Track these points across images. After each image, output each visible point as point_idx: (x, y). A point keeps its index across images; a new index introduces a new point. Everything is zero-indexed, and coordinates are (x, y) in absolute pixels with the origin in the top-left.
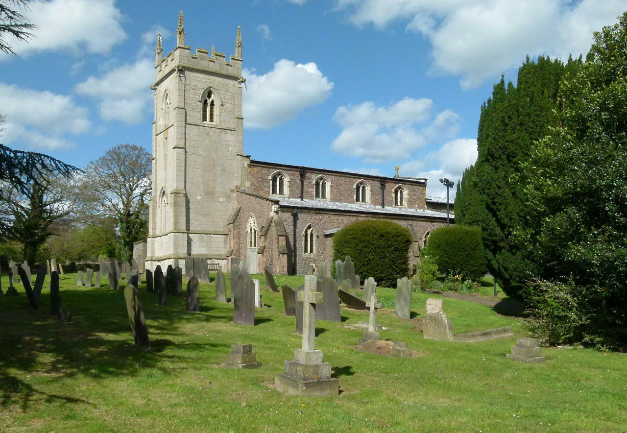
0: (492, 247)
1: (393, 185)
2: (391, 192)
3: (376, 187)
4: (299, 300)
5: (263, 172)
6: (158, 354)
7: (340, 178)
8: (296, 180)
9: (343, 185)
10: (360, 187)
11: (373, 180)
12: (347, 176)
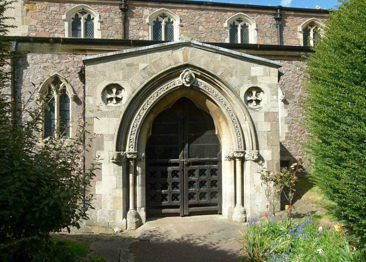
0: (50, 215)
1: (299, 20)
2: (295, 31)
3: (267, 25)
4: (121, 168)
5: (52, 9)
6: (173, 160)
7: (198, 12)
8: (113, 20)
9: (204, 24)
10: (309, 30)
11: (260, 13)
12: (210, 7)
